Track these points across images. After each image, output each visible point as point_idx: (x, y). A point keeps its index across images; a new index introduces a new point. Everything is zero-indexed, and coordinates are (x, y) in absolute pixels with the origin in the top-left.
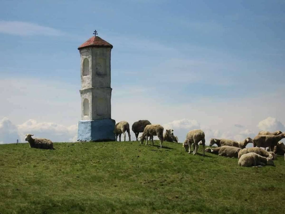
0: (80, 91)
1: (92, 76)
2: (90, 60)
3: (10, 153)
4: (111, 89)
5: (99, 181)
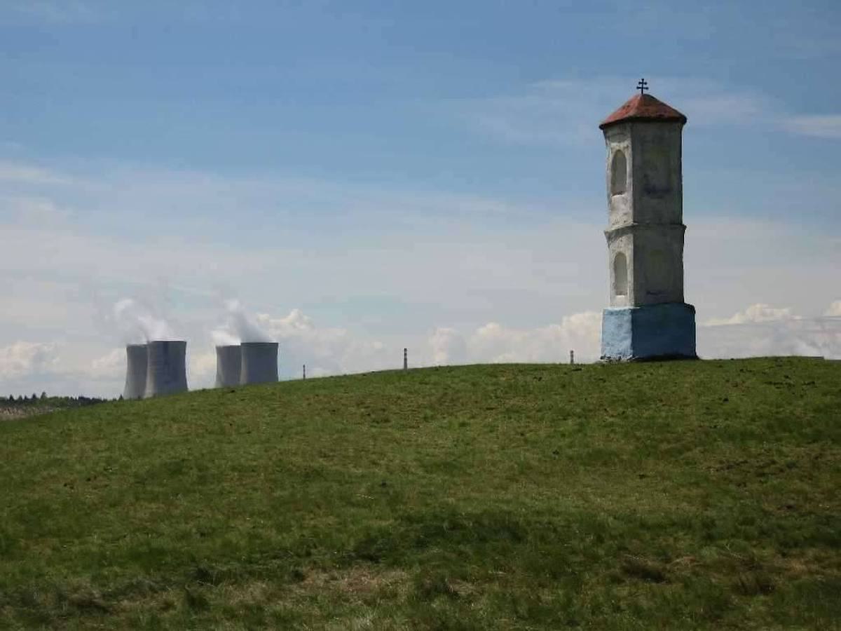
0: (606, 233)
1: (634, 195)
2: (628, 155)
3: (410, 393)
4: (684, 227)
5: (605, 464)
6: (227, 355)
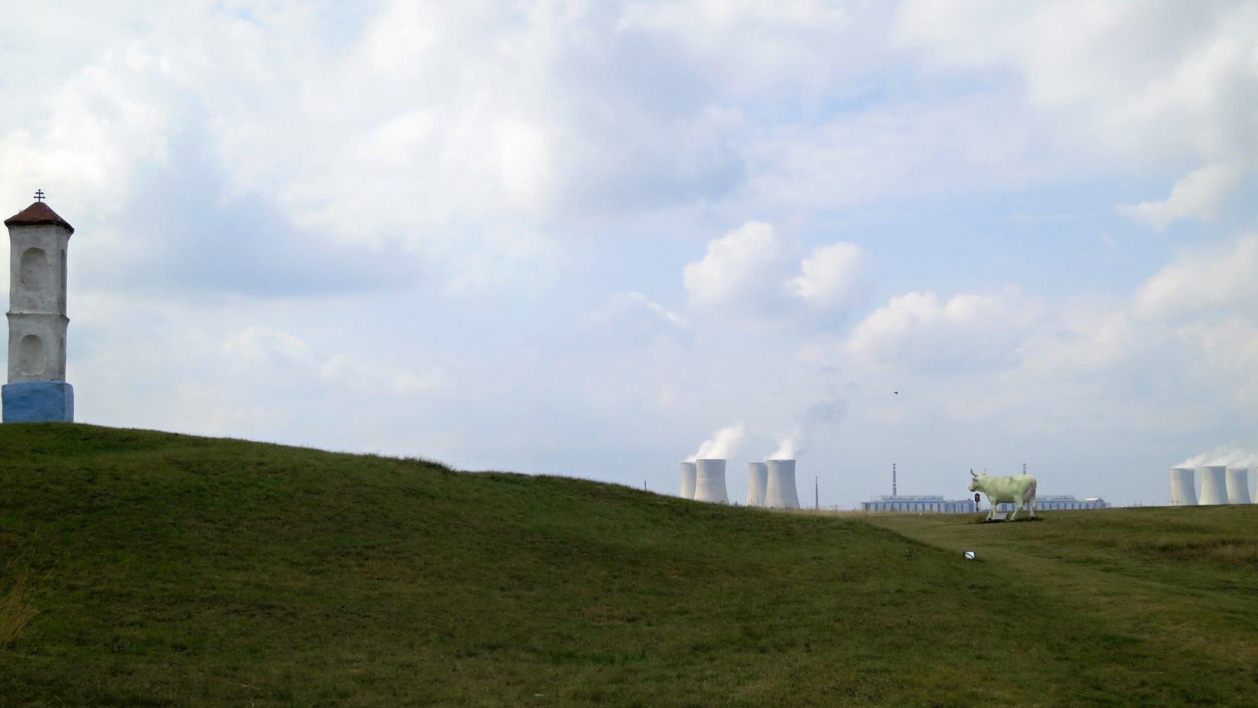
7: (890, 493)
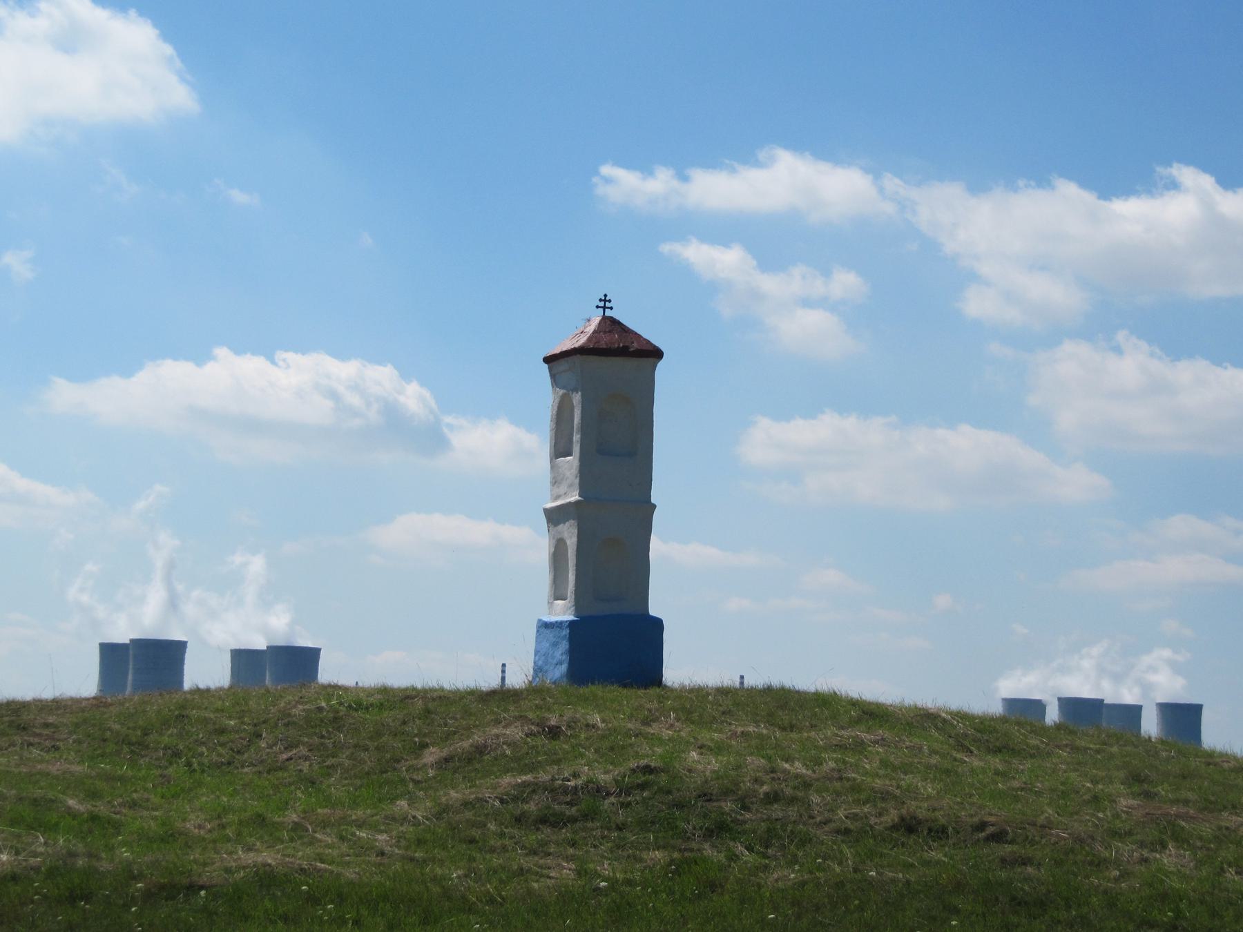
4: (654, 506)
6: (244, 660)
7: (737, 684)
